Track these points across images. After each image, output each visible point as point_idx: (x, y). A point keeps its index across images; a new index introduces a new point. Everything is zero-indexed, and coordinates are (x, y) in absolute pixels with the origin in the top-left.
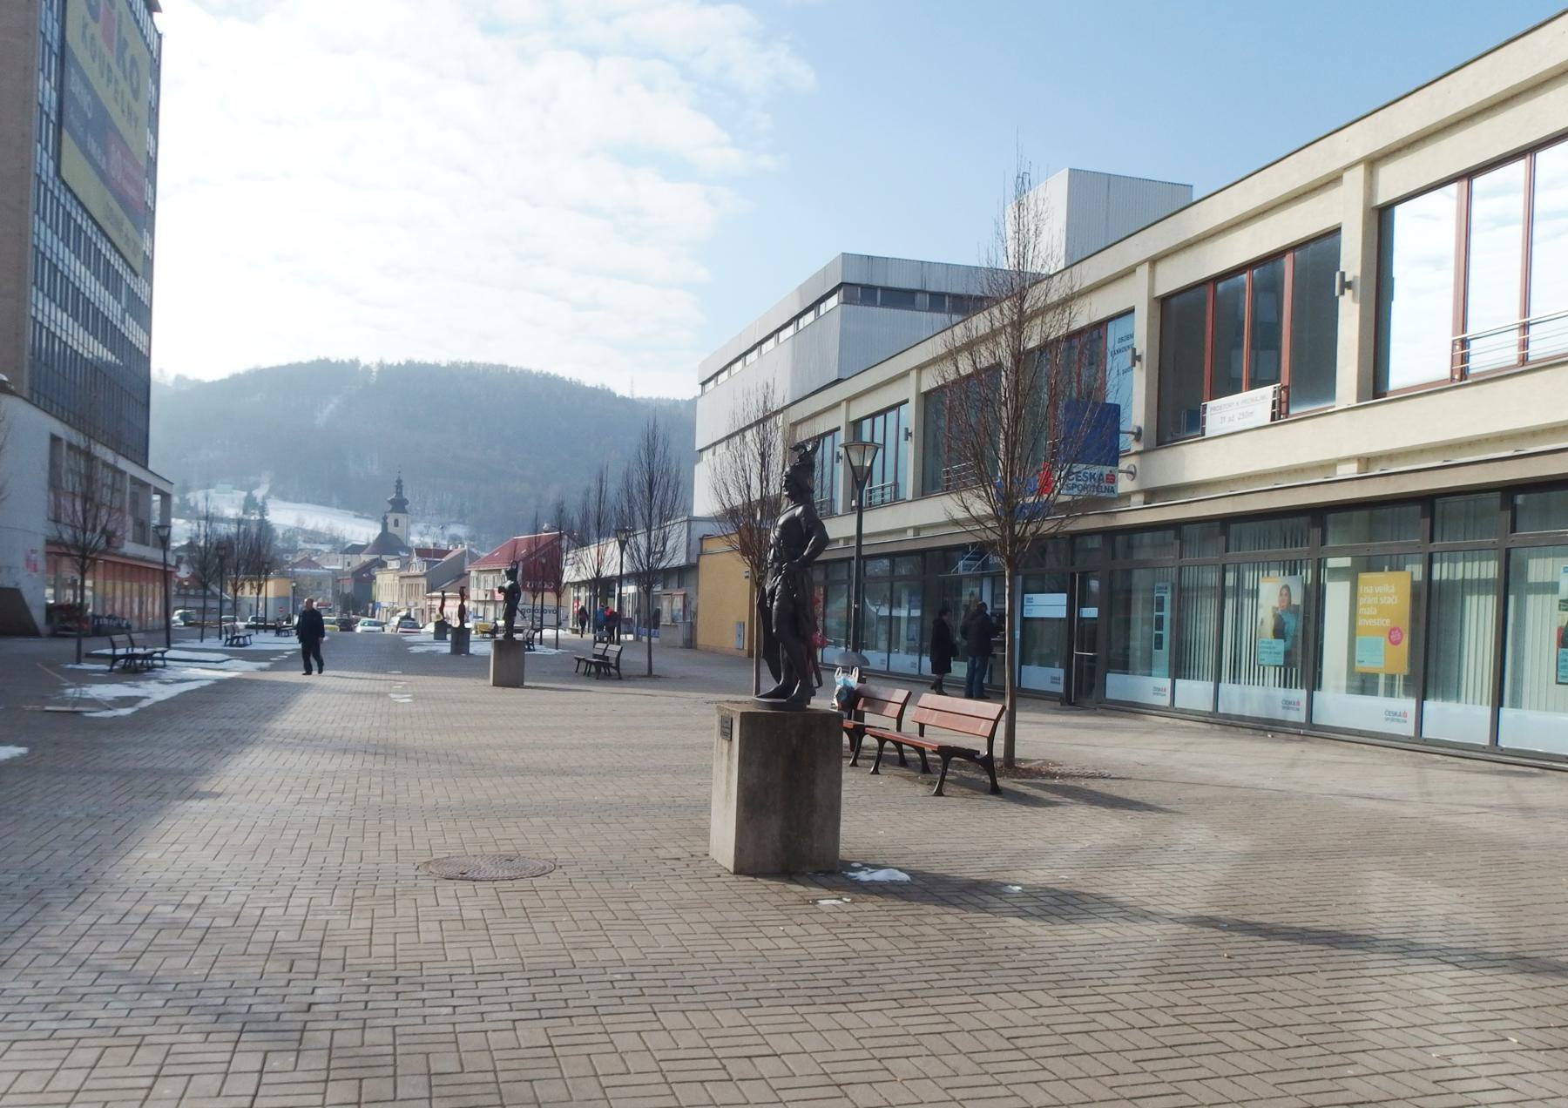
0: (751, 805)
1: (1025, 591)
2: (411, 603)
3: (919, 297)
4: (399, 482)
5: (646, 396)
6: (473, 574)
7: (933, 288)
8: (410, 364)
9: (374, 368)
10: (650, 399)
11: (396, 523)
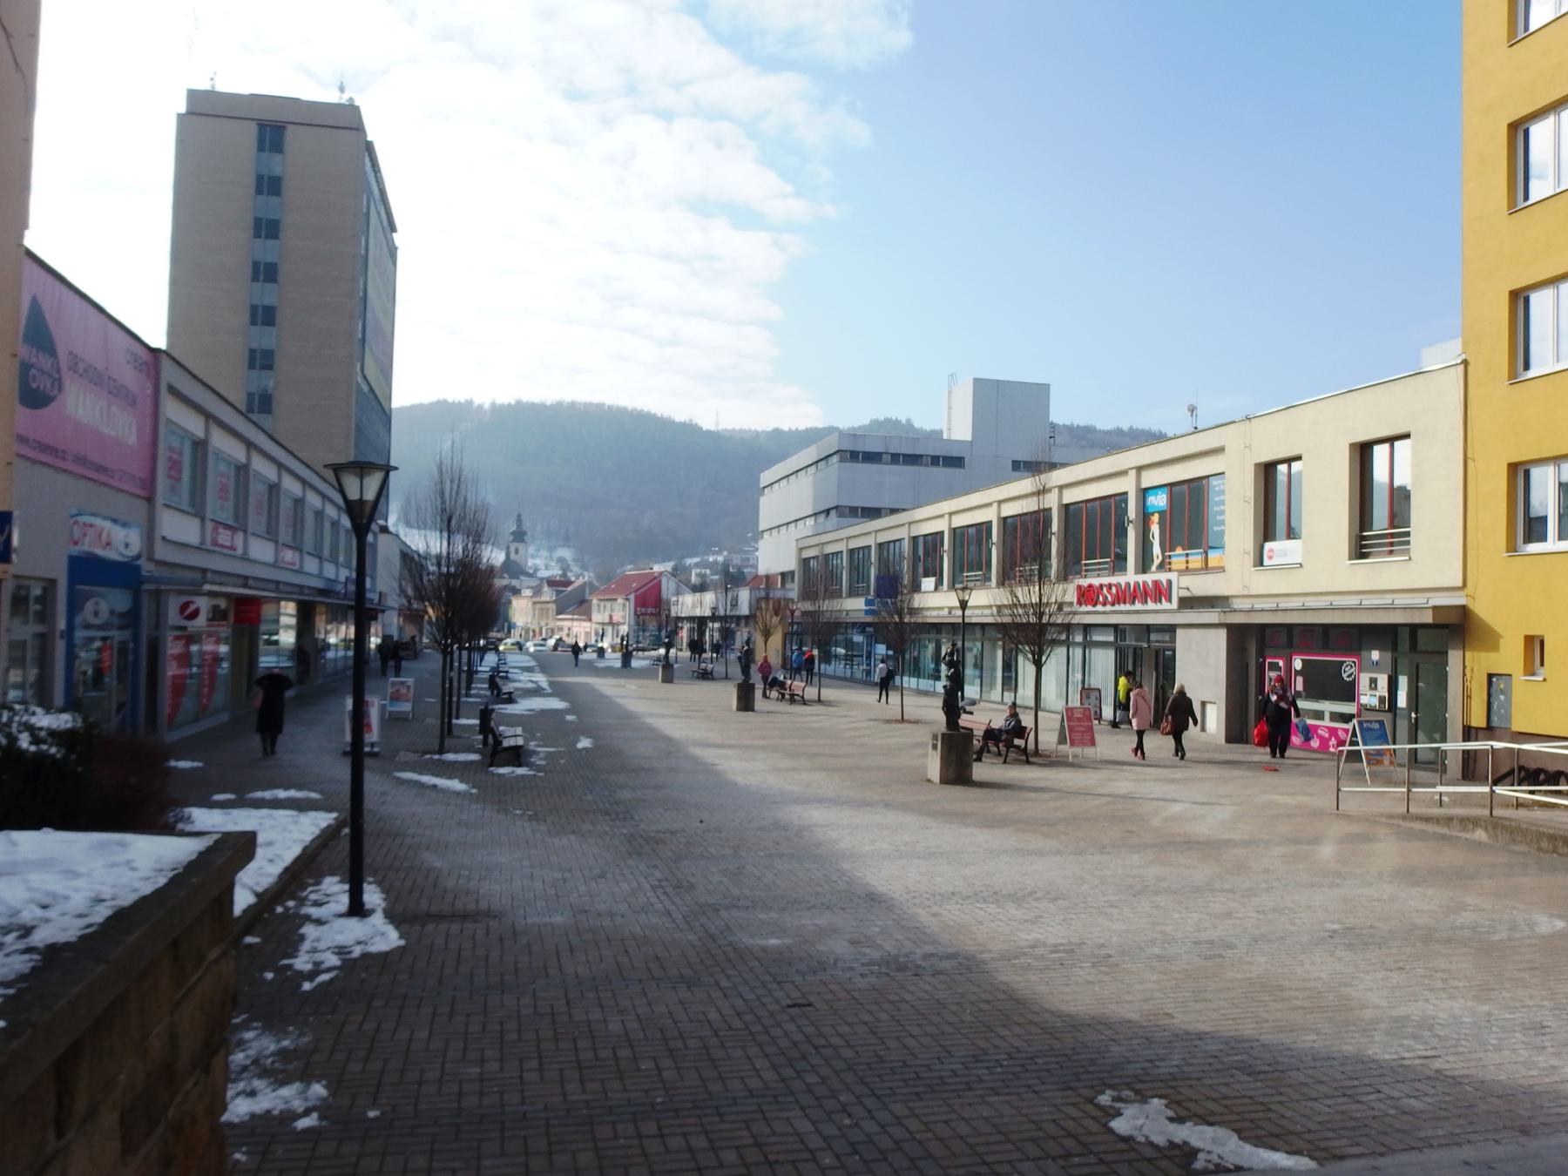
0: (739, 699)
1: (876, 642)
2: (543, 624)
3: (884, 456)
4: (519, 516)
5: (730, 427)
6: (595, 602)
7: (892, 451)
8: (519, 403)
9: (487, 406)
10: (734, 430)
11: (517, 551)
